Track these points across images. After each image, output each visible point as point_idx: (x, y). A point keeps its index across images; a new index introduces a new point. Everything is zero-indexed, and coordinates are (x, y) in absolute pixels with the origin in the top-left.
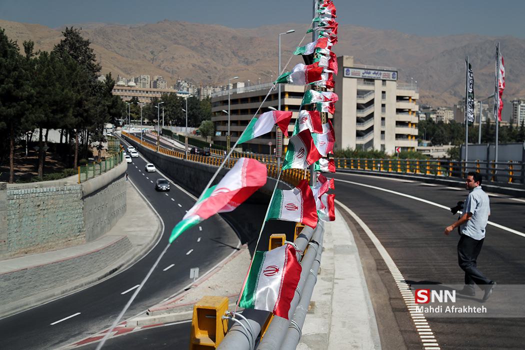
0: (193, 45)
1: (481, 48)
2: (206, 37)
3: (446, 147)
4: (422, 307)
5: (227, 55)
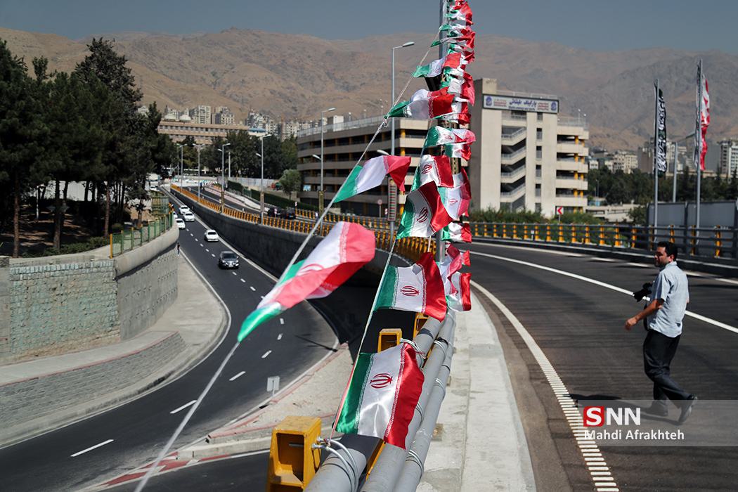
0: (271, 63)
1: (677, 68)
2: (290, 51)
3: (627, 207)
4: (594, 432)
5: (319, 77)
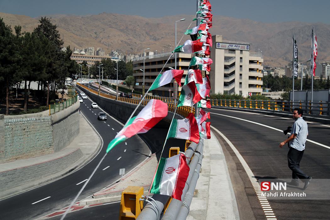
0: (121, 28)
1: (303, 30)
2: (130, 23)
3: (280, 93)
4: (265, 193)
5: (143, 34)
